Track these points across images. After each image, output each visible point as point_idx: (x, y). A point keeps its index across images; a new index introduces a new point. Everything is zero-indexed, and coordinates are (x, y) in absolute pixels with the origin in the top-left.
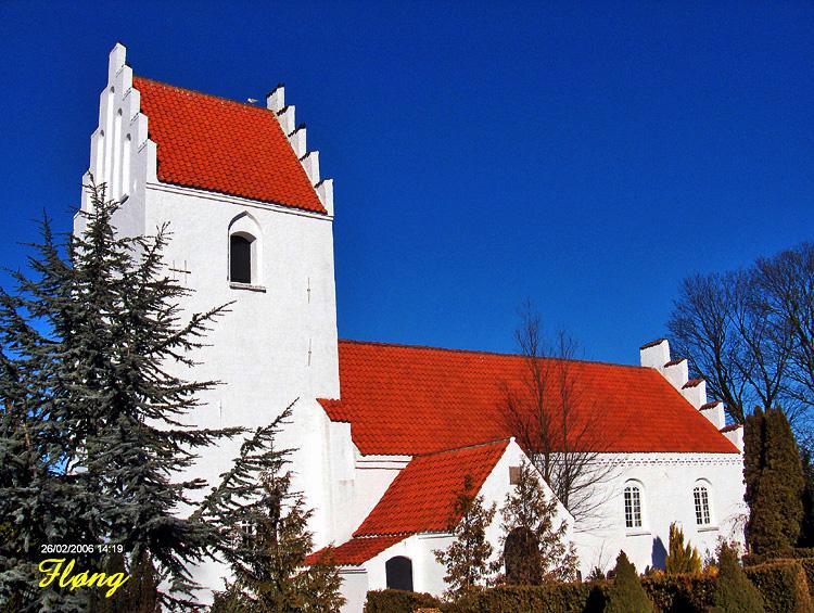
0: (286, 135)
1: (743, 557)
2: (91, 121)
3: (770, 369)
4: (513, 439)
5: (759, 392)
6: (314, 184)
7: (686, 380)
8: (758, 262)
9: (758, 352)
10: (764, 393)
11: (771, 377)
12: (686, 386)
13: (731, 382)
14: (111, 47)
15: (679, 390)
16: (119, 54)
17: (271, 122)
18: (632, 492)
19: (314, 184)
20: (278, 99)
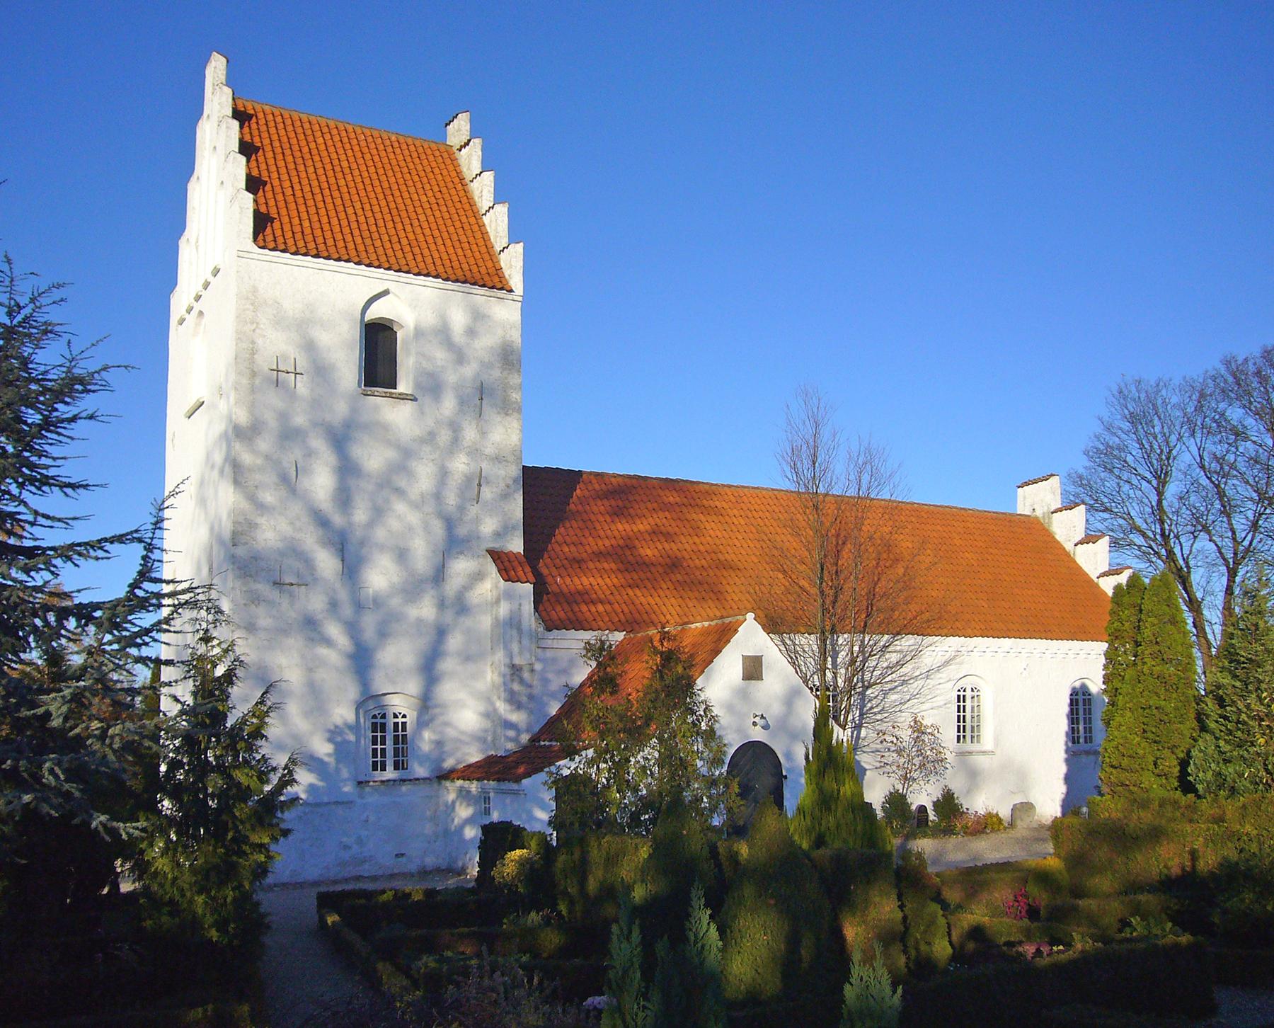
0: (467, 181)
1: (977, 933)
2: (186, 166)
3: (1240, 523)
4: (750, 616)
5: (1220, 553)
6: (498, 248)
7: (1080, 535)
8: (1227, 363)
9: (284, 479)
10: (1229, 555)
11: (1240, 535)
12: (1081, 543)
13: (1177, 537)
14: (207, 60)
15: (1069, 546)
16: (216, 68)
17: (449, 157)
18: (969, 694)
19: (498, 248)
20: (459, 129)
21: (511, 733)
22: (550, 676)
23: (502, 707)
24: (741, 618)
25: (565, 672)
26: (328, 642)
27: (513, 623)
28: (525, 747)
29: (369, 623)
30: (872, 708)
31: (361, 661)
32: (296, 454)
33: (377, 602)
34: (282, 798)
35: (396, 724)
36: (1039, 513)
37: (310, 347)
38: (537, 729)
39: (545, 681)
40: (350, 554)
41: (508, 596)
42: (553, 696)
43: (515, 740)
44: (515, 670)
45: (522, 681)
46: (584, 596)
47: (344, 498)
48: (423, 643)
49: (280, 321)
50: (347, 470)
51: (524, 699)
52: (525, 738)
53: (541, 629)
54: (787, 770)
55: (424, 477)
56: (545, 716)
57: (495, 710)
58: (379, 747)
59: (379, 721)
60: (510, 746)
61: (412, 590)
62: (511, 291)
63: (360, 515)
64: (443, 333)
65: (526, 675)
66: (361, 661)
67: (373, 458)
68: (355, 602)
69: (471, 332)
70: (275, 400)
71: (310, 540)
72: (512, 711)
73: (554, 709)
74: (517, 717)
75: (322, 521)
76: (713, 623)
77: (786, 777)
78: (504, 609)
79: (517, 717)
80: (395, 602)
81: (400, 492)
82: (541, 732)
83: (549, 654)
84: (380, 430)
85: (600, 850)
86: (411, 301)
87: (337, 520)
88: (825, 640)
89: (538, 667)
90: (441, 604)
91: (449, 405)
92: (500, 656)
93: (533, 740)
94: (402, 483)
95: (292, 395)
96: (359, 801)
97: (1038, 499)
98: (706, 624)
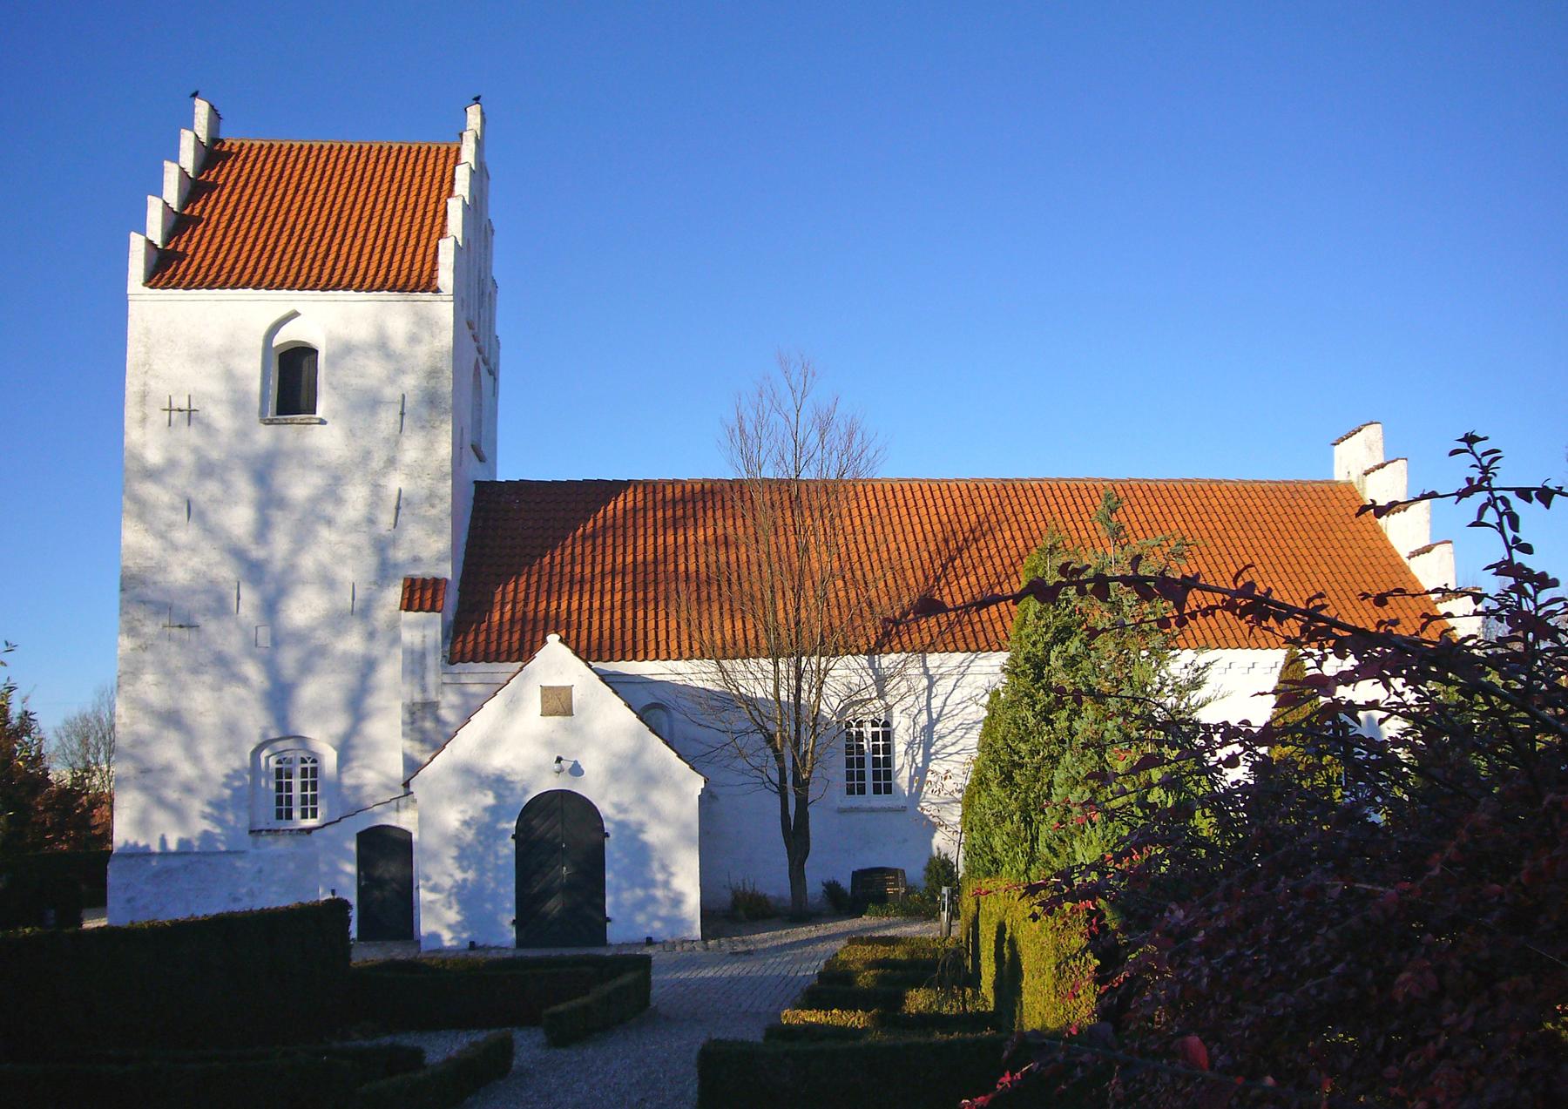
26: (243, 681)
29: (289, 659)
30: (945, 747)
31: (279, 697)
32: (213, 487)
33: (299, 637)
34: (1405, 797)
35: (304, 771)
36: (1353, 478)
37: (230, 376)
40: (273, 589)
47: (263, 529)
48: (346, 678)
49: (199, 357)
50: (269, 502)
55: (356, 496)
58: (309, 793)
59: (309, 765)
61: (337, 621)
62: (437, 291)
63: (281, 543)
64: (382, 346)
66: (279, 697)
67: (300, 487)
68: (274, 639)
69: (414, 339)
70: (191, 435)
71: (226, 573)
75: (237, 554)
80: (322, 636)
81: (329, 522)
84: (304, 458)
86: (323, 317)
87: (257, 553)
90: (371, 636)
91: (387, 420)
94: (329, 509)
95: (208, 428)
96: (253, 851)
97: (1356, 461)
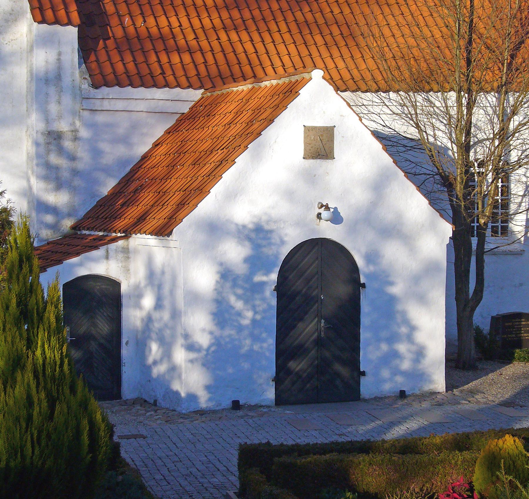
4: (317, 74)
21: (49, 219)
22: (105, 146)
23: (38, 186)
24: (306, 75)
25: (125, 140)
27: (48, 82)
28: (66, 236)
38: (82, 213)
39: (96, 153)
41: (44, 41)
42: (107, 171)
43: (54, 227)
44: (53, 138)
45: (61, 151)
46: (164, 42)
51: (65, 175)
52: (68, 224)
53: (86, 86)
54: (367, 276)
56: (93, 196)
57: (30, 188)
60: (46, 234)
65: (68, 144)
72: (47, 190)
73: (108, 186)
74: (59, 199)
76: (281, 82)
77: (363, 286)
78: (43, 59)
79: (59, 199)
82: (88, 216)
83: (101, 118)
85: (466, 9)
88: (466, 196)
89: (84, 133)
92: (35, 122)
93: (75, 227)
98: (274, 82)
